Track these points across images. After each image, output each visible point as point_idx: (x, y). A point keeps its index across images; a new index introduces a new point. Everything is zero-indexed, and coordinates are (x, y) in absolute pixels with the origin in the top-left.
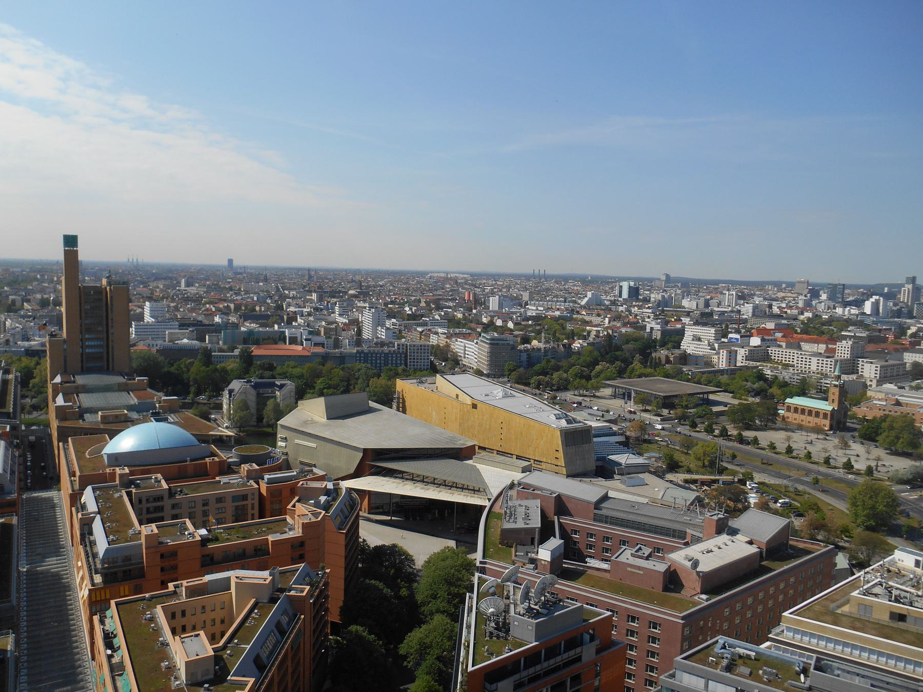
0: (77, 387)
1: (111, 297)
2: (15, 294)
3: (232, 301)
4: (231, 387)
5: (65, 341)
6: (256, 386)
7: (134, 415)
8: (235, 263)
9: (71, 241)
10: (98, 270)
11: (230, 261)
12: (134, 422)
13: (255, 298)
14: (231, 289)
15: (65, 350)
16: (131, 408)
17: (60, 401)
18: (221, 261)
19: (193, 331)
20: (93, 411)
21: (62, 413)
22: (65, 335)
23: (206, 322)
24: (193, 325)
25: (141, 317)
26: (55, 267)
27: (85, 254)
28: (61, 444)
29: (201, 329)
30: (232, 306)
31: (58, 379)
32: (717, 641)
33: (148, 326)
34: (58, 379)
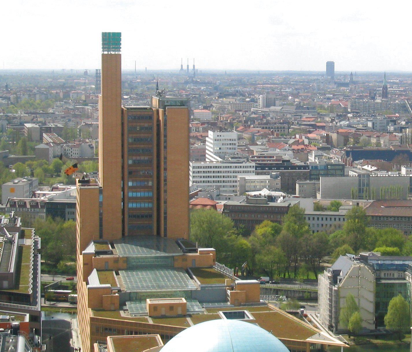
0: (116, 260)
1: (165, 125)
2: (32, 121)
3: (336, 129)
4: (336, 266)
5: (101, 191)
6: (378, 269)
7: (196, 307)
8: (338, 68)
9: (111, 41)
10: (154, 83)
11: (330, 65)
12: (199, 319)
13: (370, 124)
14: (331, 109)
15: (101, 204)
16: (190, 295)
17: (94, 280)
18: (308, 70)
19: (276, 177)
20: (139, 298)
21: (98, 301)
22: (100, 184)
23: (297, 162)
24: (278, 167)
25: (201, 156)
26: (82, 80)
27: (131, 62)
28: (96, 345)
29: (289, 175)
30: (334, 136)
31: (91, 249)
32: (221, 276)
33: (216, 170)
34: (91, 249)
